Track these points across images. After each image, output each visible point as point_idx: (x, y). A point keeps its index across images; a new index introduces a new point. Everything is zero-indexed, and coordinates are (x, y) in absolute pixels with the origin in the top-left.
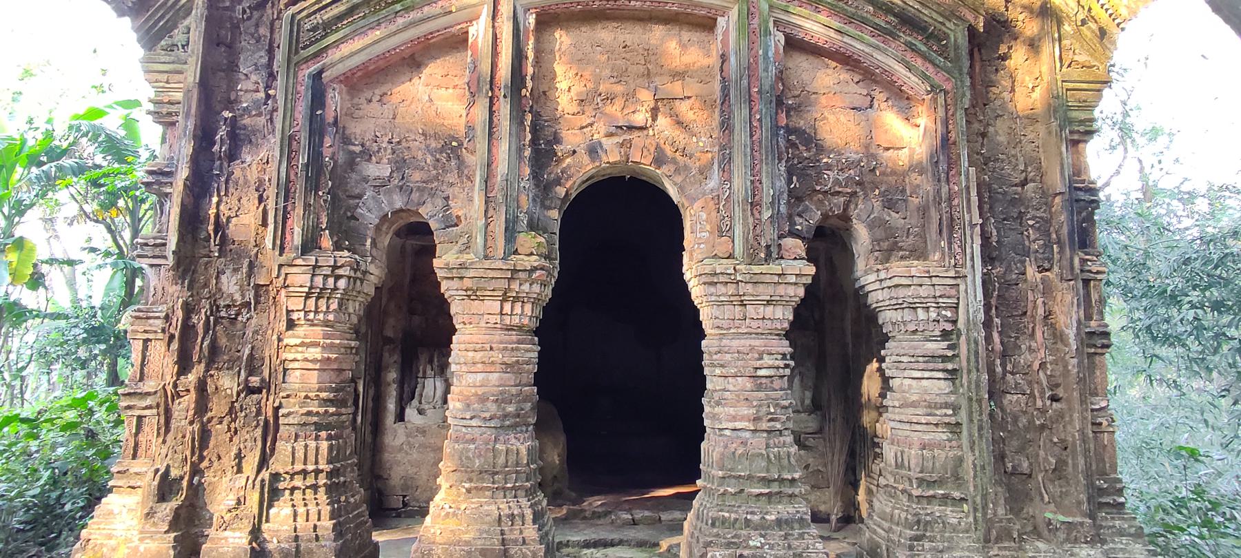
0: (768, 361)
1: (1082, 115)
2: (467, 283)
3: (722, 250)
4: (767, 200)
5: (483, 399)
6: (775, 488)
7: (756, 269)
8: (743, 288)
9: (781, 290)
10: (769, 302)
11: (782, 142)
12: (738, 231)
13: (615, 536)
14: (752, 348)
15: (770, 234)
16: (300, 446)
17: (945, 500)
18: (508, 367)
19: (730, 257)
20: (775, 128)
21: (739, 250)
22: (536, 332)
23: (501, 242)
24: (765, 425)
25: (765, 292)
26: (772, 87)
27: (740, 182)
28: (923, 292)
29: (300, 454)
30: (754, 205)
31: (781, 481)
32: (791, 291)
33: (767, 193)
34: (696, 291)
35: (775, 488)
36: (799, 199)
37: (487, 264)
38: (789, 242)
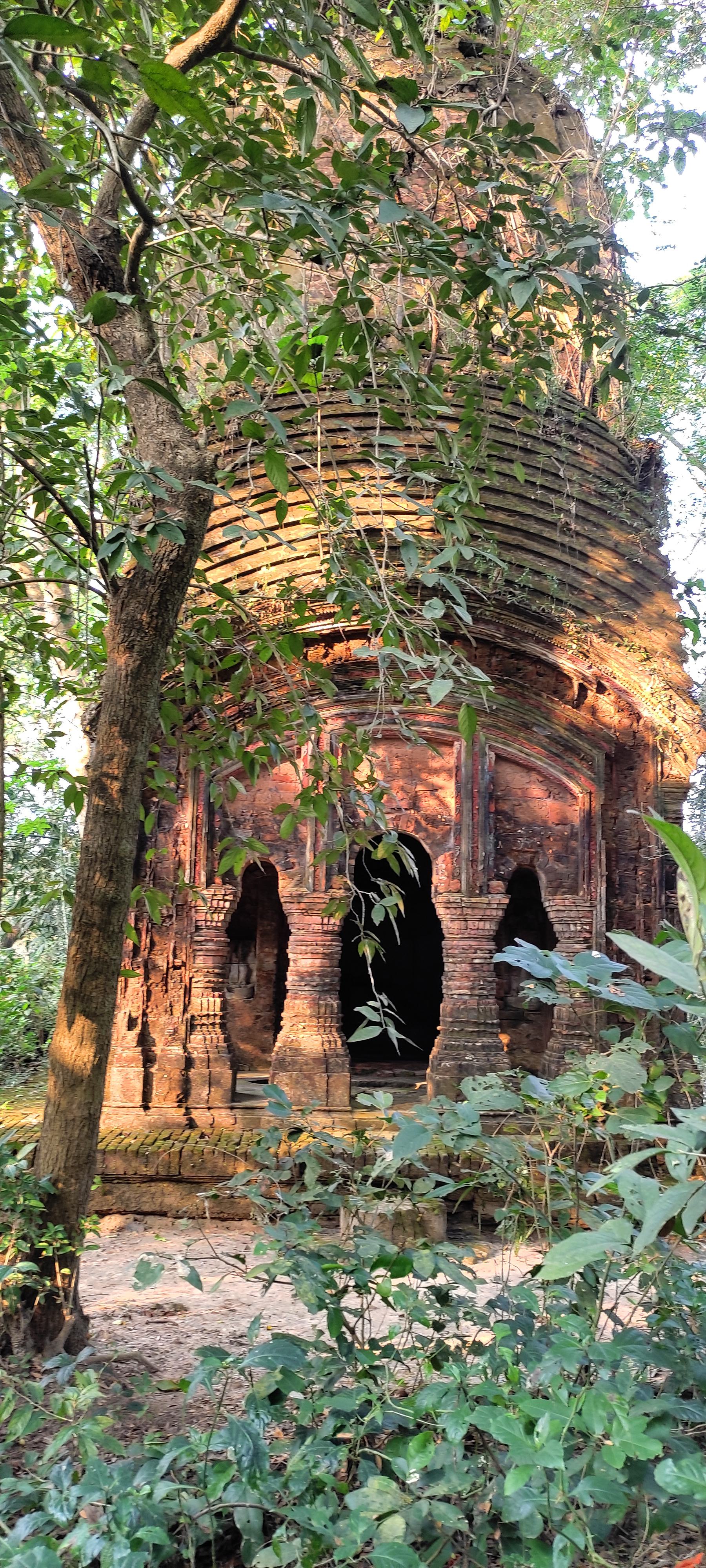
0: (480, 954)
1: (674, 807)
2: (303, 906)
3: (452, 888)
4: (481, 859)
5: (311, 974)
6: (482, 1028)
7: (473, 900)
8: (466, 911)
9: (488, 912)
10: (481, 920)
11: (492, 822)
12: (464, 877)
13: (382, 1080)
14: (471, 947)
15: (481, 880)
16: (205, 1000)
17: (581, 1036)
18: (326, 956)
19: (459, 892)
20: (487, 813)
21: (464, 888)
22: (340, 934)
23: (323, 882)
24: (477, 992)
25: (479, 914)
26: (487, 788)
27: (465, 847)
28: (572, 914)
29: (205, 1005)
30: (473, 862)
31: (485, 1024)
32: (494, 913)
33: (481, 854)
34: (440, 911)
35: (482, 1028)
36: (503, 855)
37: (315, 895)
38: (494, 883)
